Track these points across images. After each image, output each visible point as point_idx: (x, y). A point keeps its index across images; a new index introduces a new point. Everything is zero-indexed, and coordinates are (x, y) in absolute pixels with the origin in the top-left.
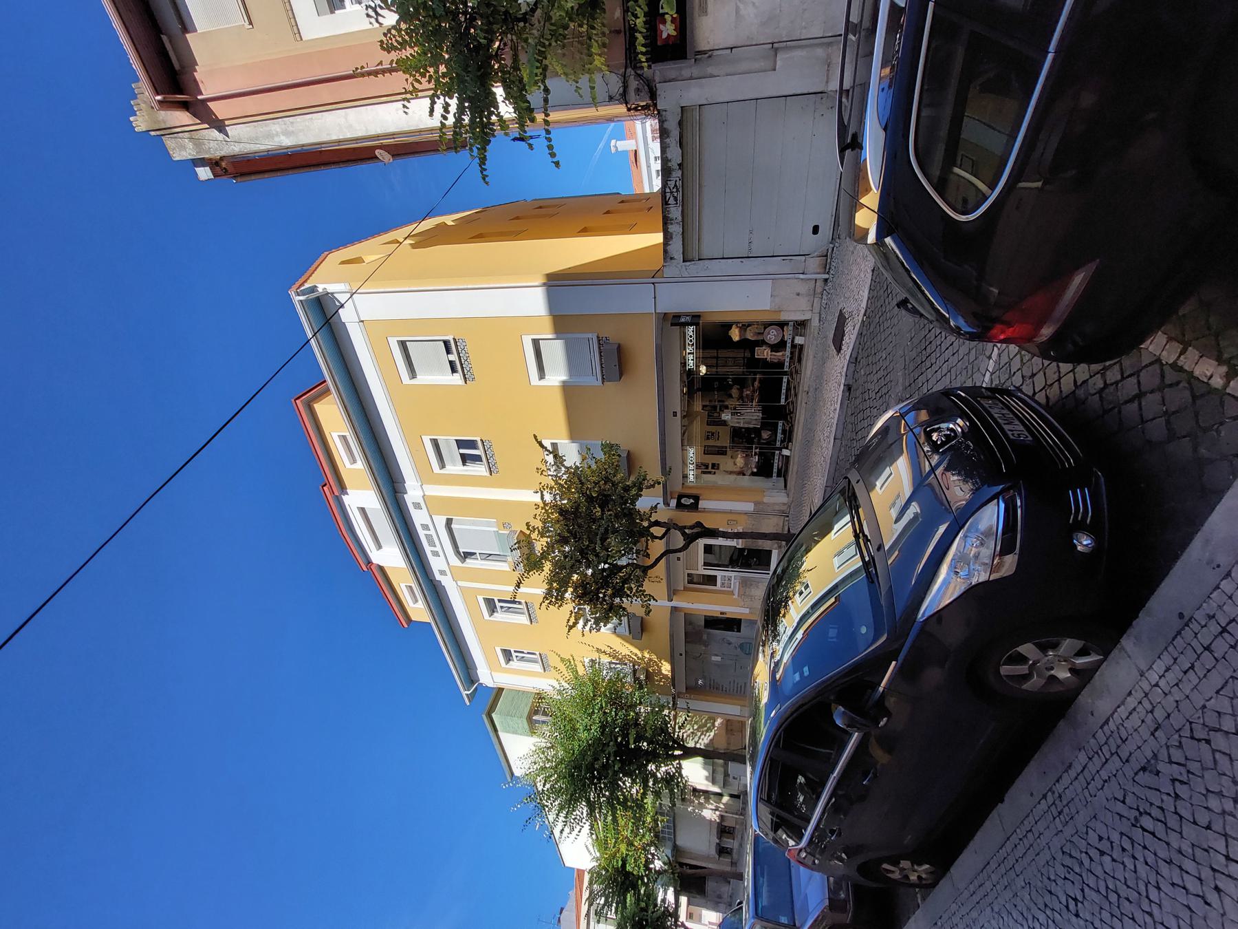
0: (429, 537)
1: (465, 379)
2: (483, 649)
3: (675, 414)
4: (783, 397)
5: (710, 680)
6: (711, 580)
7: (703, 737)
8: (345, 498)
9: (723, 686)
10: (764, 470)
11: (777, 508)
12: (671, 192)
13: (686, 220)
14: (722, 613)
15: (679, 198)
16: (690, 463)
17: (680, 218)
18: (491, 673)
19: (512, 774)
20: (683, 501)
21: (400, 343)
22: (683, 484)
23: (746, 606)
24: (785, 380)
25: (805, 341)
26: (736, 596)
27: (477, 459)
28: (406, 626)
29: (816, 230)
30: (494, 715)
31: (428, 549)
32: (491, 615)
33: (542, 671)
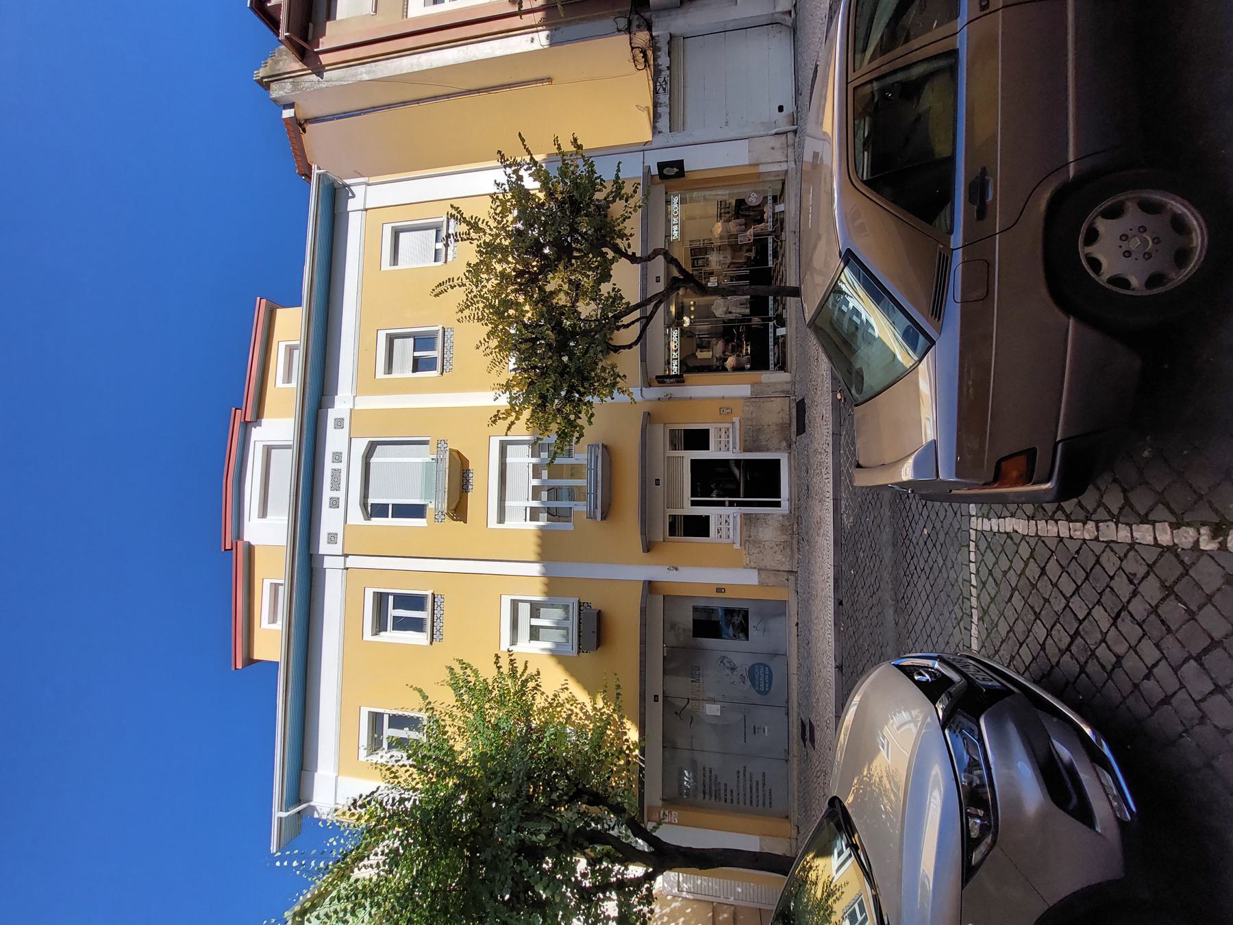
0: (336, 472)
2: (342, 704)
3: (656, 698)
4: (770, 258)
5: (704, 768)
6: (698, 527)
9: (726, 785)
10: (759, 362)
11: (779, 388)
12: (661, 85)
13: (672, 103)
15: (668, 88)
17: (668, 102)
18: (336, 778)
20: (665, 171)
23: (752, 564)
24: (770, 240)
25: (787, 332)
27: (417, 625)
28: (239, 666)
29: (781, 109)
31: (327, 493)
32: (376, 633)
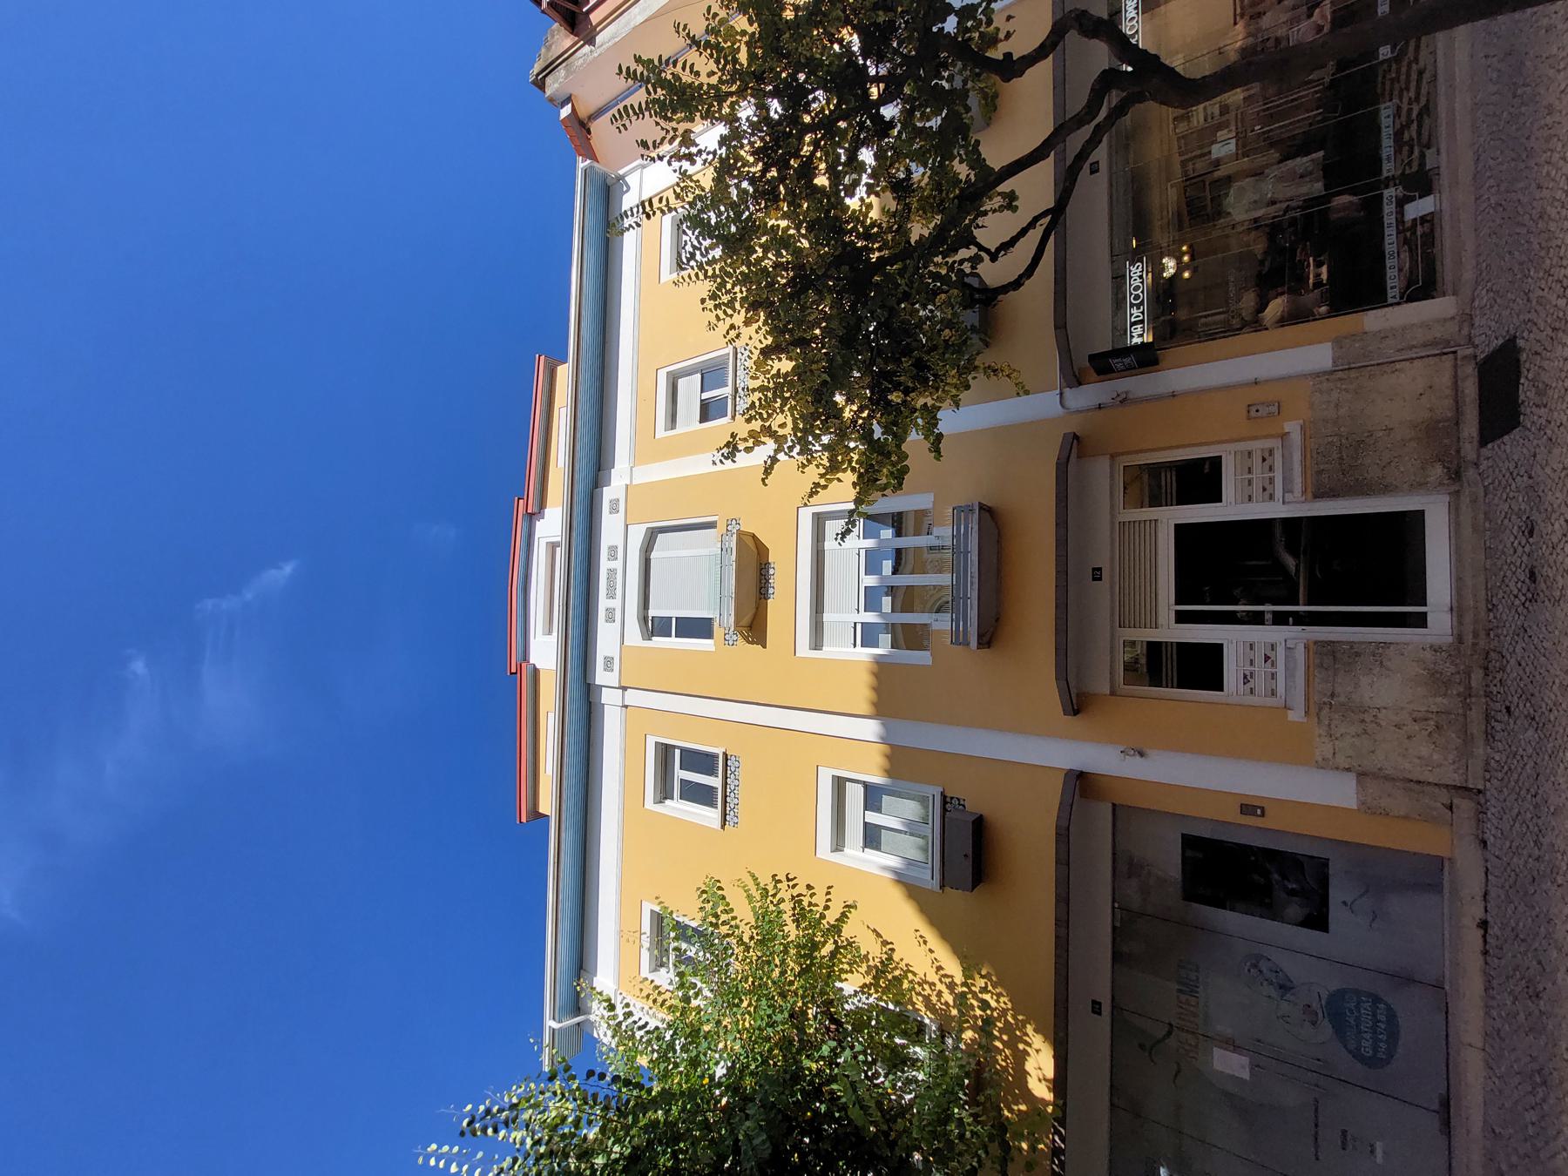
1: (724, 820)
3: (1096, 1008)
14: (1248, 809)
16: (1132, 305)
21: (660, 747)
28: (524, 820)
31: (603, 603)
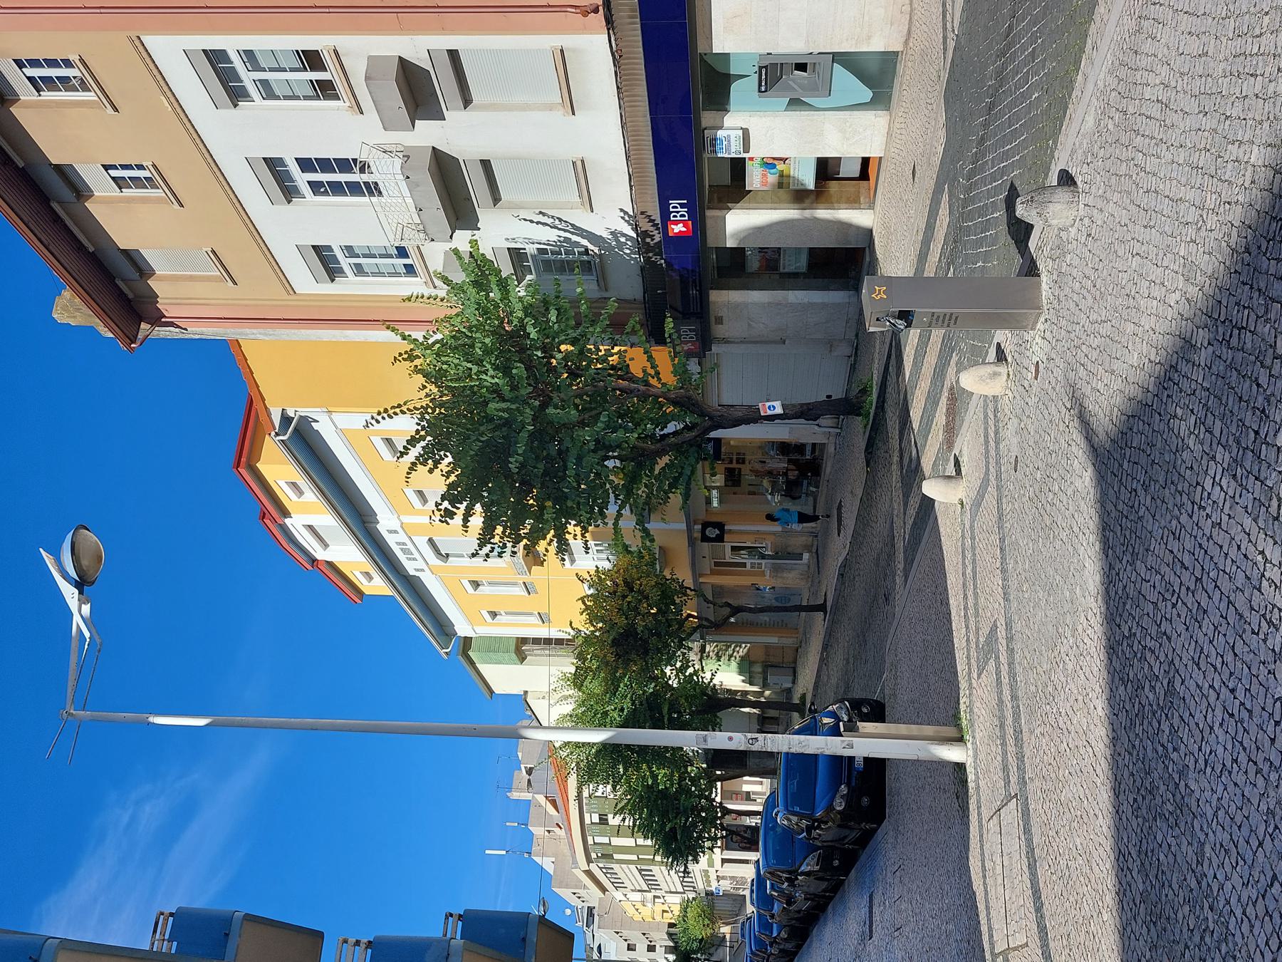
7: (738, 649)
8: (288, 521)
19: (492, 692)
22: (707, 510)
26: (767, 577)
30: (470, 653)
33: (526, 594)
